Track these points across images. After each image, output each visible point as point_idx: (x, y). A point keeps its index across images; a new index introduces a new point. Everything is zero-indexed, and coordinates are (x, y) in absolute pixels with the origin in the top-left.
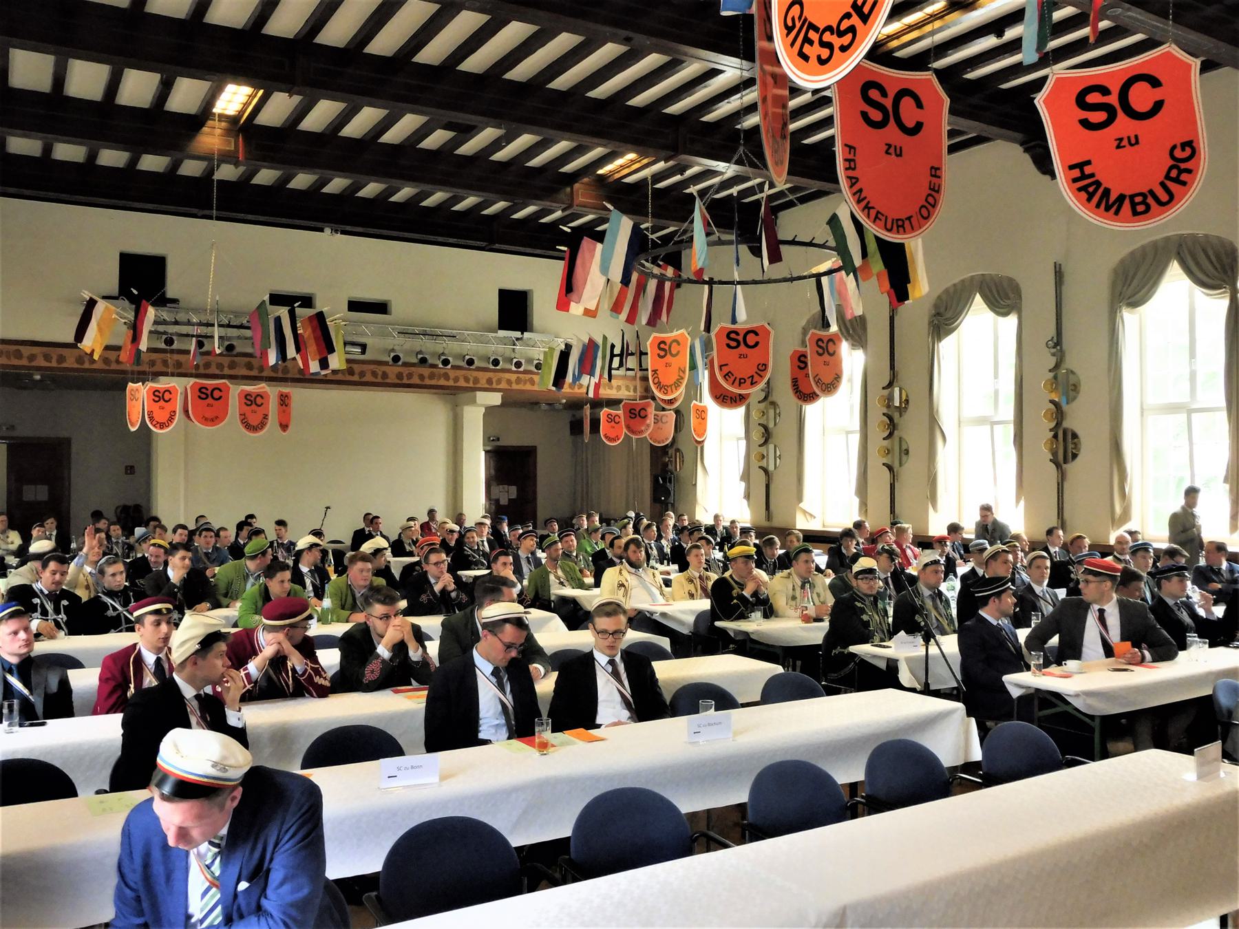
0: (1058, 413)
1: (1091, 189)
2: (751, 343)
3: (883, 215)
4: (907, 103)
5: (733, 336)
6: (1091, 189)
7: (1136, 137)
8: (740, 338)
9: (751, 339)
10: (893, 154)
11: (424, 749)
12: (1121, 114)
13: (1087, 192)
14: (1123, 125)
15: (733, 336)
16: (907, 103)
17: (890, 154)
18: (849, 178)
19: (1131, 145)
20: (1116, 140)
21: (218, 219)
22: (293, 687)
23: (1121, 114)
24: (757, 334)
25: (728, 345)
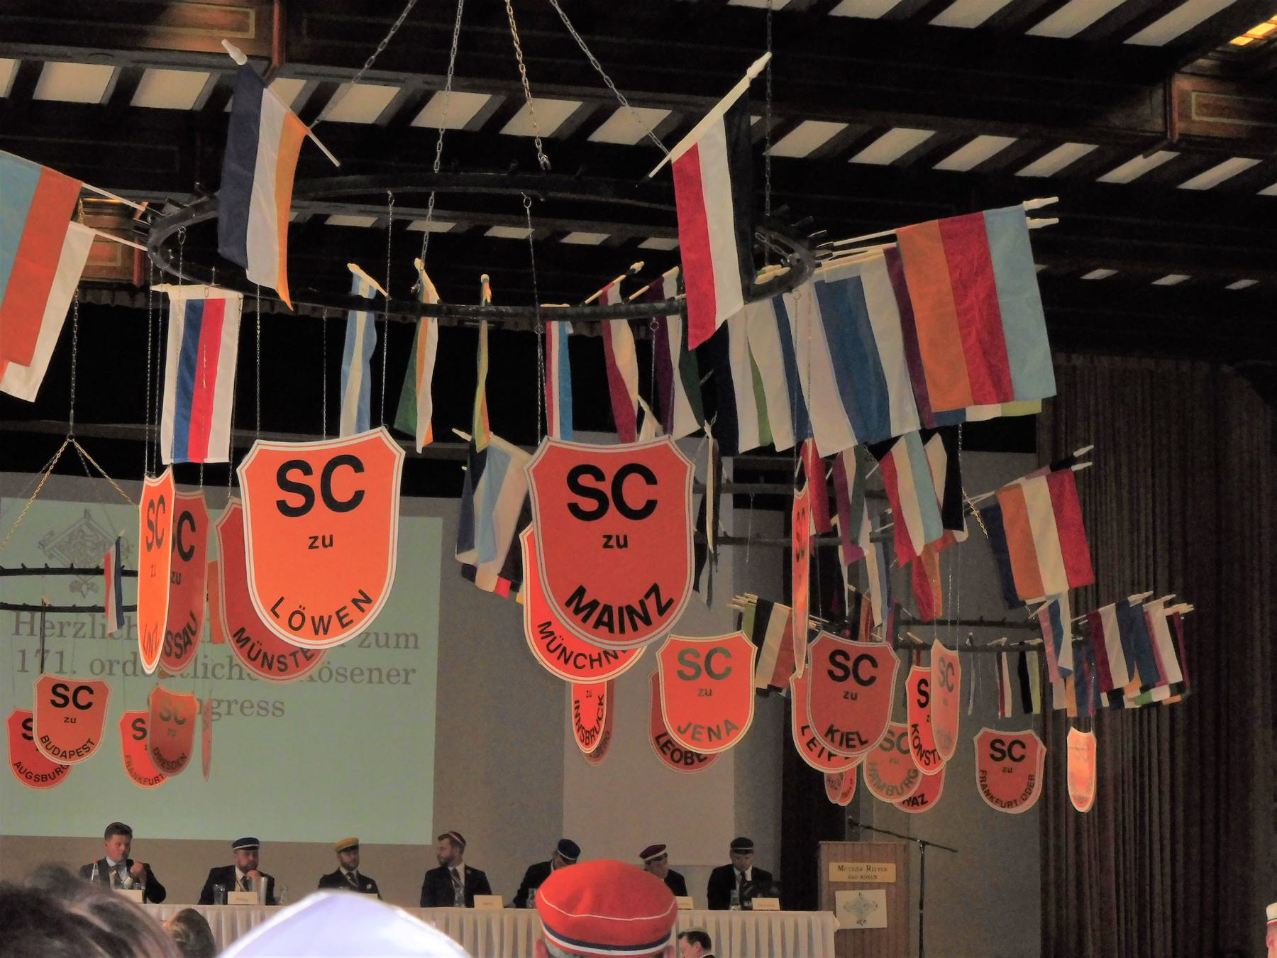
0: (1159, 787)
1: (605, 619)
2: (82, 702)
3: (852, 733)
4: (865, 664)
5: (60, 690)
6: (605, 619)
7: (625, 538)
8: (70, 695)
9: (83, 698)
10: (850, 698)
11: (419, 904)
12: (851, 677)
13: (604, 624)
14: (851, 683)
15: (60, 690)
16: (865, 664)
17: (848, 698)
18: (982, 785)
19: (853, 699)
20: (604, 536)
21: (159, 423)
22: (550, 868)
23: (851, 677)
24: (91, 691)
25: (53, 703)
